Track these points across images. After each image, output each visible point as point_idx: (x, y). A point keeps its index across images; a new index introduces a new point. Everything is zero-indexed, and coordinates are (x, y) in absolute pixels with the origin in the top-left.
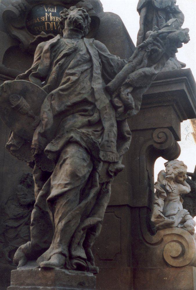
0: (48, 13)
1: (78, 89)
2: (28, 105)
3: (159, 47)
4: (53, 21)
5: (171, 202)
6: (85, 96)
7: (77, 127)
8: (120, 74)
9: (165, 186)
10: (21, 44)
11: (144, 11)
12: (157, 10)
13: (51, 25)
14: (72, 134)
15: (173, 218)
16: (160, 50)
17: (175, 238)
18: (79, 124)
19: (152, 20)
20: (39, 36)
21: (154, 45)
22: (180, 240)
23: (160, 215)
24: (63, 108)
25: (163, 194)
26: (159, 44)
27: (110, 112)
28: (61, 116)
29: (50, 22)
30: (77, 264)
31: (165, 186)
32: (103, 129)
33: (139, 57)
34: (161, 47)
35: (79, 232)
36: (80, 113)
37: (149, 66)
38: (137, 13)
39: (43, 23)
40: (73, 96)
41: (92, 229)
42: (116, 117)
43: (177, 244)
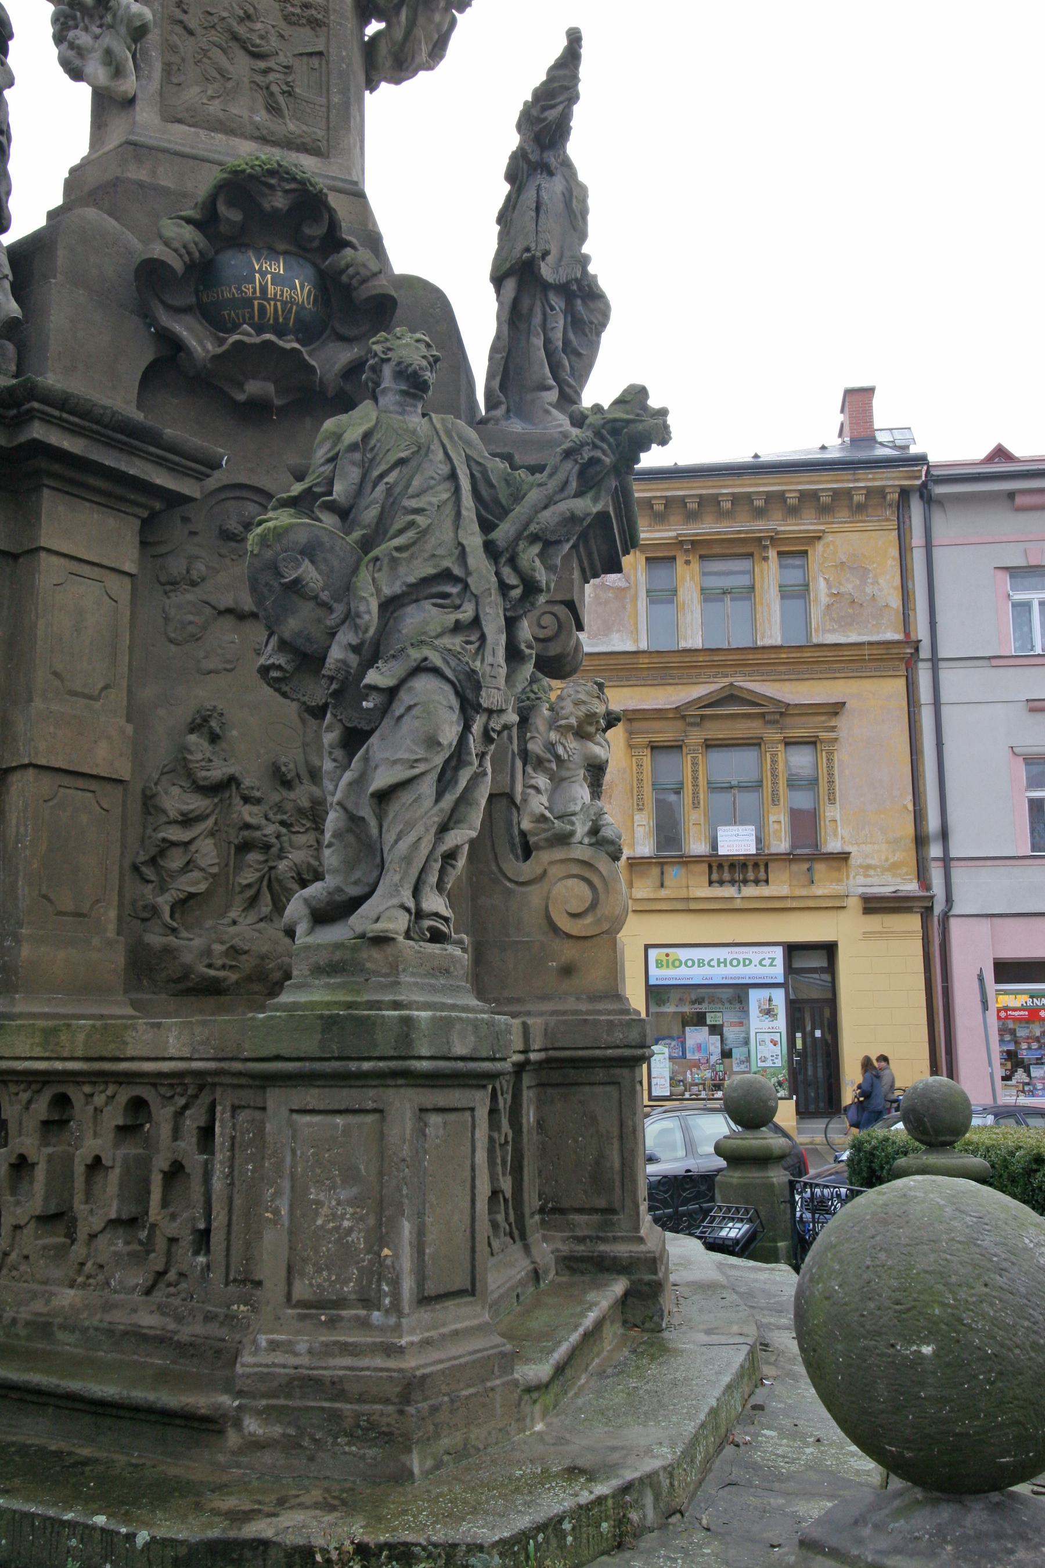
0: (263, 275)
1: (428, 547)
2: (319, 577)
3: (604, 452)
4: (275, 299)
5: (565, 784)
6: (447, 563)
7: (433, 634)
8: (520, 511)
9: (553, 745)
10: (182, 354)
11: (510, 285)
12: (546, 286)
13: (270, 309)
14: (427, 652)
15: (573, 824)
16: (607, 460)
17: (575, 870)
18: (434, 628)
19: (531, 310)
20: (236, 337)
21: (595, 447)
22: (587, 874)
23: (543, 816)
24: (397, 588)
25: (547, 764)
26: (605, 446)
27: (495, 597)
28: (391, 606)
29: (268, 300)
30: (431, 929)
31: (553, 745)
32: (483, 638)
33: (561, 476)
34: (609, 452)
35: (436, 861)
36: (434, 601)
37: (578, 495)
38: (490, 289)
39: (248, 302)
40: (419, 560)
41: (450, 856)
42: (505, 610)
43: (582, 884)
